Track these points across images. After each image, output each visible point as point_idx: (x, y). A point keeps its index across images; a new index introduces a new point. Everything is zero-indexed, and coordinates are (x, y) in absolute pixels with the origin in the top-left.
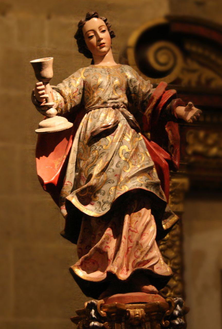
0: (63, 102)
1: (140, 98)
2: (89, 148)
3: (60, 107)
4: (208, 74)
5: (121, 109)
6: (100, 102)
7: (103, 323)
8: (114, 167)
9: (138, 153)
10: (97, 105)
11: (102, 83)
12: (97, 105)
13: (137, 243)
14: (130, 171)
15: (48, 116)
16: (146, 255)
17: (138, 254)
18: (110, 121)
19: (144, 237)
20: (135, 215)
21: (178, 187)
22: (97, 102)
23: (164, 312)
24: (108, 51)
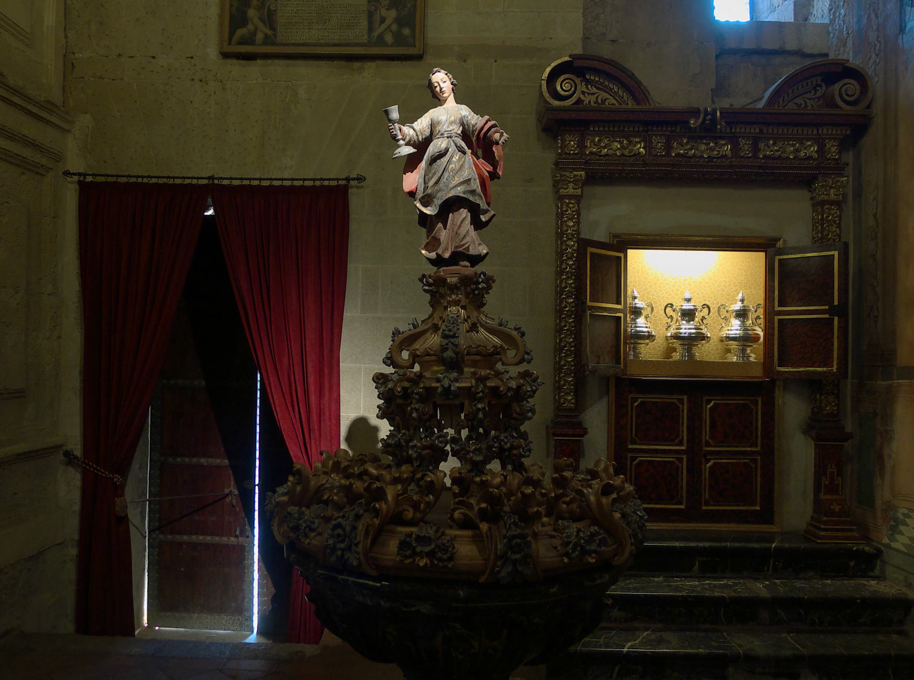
0: (415, 135)
2: (430, 167)
5: (453, 138)
8: (445, 180)
10: (438, 136)
12: (438, 136)
13: (457, 233)
14: (457, 180)
15: (399, 146)
16: (462, 240)
17: (457, 240)
18: (444, 146)
19: (461, 228)
21: (578, 178)
22: (438, 134)
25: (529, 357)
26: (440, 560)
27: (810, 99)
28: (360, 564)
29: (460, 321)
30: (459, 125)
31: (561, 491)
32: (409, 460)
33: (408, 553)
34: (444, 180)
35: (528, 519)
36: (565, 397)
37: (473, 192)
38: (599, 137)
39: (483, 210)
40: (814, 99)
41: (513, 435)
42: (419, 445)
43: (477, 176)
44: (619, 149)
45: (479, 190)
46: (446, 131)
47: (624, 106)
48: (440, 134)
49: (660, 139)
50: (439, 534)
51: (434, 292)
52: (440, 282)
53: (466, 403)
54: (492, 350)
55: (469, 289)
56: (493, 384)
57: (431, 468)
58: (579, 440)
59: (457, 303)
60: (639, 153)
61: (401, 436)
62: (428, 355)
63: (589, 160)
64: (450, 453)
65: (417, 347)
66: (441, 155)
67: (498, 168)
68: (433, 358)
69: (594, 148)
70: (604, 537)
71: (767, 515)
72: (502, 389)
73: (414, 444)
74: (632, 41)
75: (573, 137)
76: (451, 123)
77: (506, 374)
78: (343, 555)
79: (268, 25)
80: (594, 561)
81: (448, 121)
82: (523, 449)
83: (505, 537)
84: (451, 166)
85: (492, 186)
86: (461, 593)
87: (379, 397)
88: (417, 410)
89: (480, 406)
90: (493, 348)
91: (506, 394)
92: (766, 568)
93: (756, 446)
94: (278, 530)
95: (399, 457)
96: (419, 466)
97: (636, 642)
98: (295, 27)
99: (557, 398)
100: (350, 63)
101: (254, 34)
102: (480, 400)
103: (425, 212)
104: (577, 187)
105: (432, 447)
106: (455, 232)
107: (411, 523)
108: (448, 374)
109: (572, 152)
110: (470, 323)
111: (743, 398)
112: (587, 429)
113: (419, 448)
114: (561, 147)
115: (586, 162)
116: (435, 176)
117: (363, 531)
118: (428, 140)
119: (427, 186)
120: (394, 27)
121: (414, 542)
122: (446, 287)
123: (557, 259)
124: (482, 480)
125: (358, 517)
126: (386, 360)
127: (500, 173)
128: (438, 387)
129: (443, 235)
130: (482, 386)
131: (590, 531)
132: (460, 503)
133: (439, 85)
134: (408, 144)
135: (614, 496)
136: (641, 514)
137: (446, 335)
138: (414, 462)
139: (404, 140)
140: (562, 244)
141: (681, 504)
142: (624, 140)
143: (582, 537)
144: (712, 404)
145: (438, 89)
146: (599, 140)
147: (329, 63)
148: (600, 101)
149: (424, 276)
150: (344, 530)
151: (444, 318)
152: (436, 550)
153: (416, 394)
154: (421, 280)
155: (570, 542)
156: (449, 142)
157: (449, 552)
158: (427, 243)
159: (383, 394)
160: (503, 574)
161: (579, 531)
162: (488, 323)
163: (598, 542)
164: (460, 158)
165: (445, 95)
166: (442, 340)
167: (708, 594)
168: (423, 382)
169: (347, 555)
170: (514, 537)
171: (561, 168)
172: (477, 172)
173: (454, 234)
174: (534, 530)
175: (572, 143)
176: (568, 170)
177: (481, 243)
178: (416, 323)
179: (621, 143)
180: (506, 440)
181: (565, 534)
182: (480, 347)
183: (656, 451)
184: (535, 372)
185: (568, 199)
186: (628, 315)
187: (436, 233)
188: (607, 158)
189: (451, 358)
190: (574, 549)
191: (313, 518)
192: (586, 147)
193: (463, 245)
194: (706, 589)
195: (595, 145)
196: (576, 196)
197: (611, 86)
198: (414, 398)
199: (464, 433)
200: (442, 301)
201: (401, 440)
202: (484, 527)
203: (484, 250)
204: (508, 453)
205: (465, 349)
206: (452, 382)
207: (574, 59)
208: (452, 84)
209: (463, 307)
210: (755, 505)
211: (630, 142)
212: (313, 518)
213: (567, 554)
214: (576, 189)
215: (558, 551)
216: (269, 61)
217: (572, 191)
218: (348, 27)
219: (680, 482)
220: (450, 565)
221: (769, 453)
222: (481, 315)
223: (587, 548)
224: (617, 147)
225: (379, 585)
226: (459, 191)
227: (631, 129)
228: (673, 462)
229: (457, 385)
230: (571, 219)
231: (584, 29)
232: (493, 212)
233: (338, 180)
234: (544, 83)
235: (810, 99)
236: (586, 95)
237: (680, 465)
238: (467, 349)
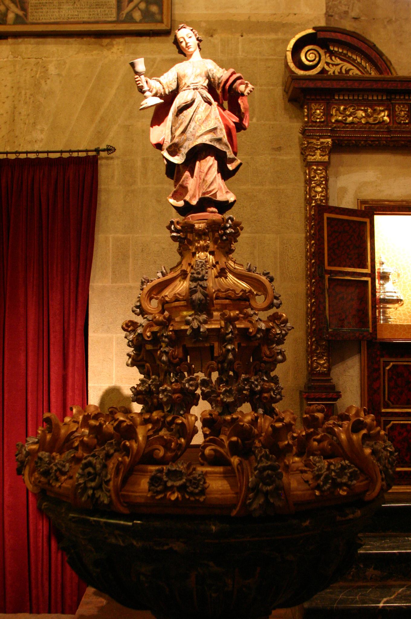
1: (217, 82)
3: (159, 91)
4: (348, 66)
5: (199, 90)
6: (186, 86)
7: (179, 233)
8: (191, 130)
9: (210, 119)
10: (184, 88)
11: (179, 74)
12: (184, 88)
13: (204, 180)
14: (203, 129)
15: (146, 97)
16: (209, 187)
17: (204, 187)
20: (203, 162)
21: (325, 145)
22: (184, 86)
23: (220, 225)
24: (195, 51)
25: (278, 302)
26: (192, 494)
28: (111, 502)
29: (208, 266)
30: (205, 78)
31: (312, 430)
32: (159, 406)
33: (160, 488)
34: (190, 129)
36: (318, 361)
37: (219, 140)
38: (344, 105)
39: (230, 158)
41: (263, 379)
42: (169, 388)
43: (223, 126)
44: (364, 117)
45: (225, 139)
46: (192, 83)
47: (367, 75)
48: (186, 86)
49: (403, 107)
50: (191, 470)
51: (182, 238)
52: (188, 228)
53: (216, 345)
54: (241, 294)
55: (217, 235)
56: (242, 326)
57: (182, 412)
58: (333, 404)
59: (204, 249)
60: (384, 121)
61: (152, 382)
62: (177, 300)
63: (335, 127)
64: (201, 397)
65: (167, 294)
66: (187, 106)
67: (244, 119)
68: (182, 303)
69: (339, 117)
70: (354, 470)
72: (251, 330)
73: (164, 388)
74: (374, 19)
75: (318, 106)
76: (197, 76)
77: (254, 315)
78: (93, 494)
79: (19, 7)
80: (345, 493)
81: (194, 74)
82: (274, 392)
83: (256, 469)
84: (197, 116)
85: (240, 137)
86: (214, 528)
87: (129, 346)
88: (166, 353)
89: (229, 347)
90: (242, 292)
91: (255, 335)
94: (30, 480)
95: (150, 404)
96: (169, 411)
97: (392, 597)
98: (46, 7)
99: (309, 362)
100: (99, 40)
102: (230, 341)
104: (324, 154)
105: (183, 391)
106: (202, 180)
107: (162, 461)
108: (197, 316)
109: (318, 120)
110: (218, 268)
112: (340, 392)
113: (169, 391)
114: (307, 116)
115: (332, 131)
116: (182, 125)
117: (114, 469)
118: (174, 93)
119: (174, 135)
120: (143, 6)
121: (165, 477)
122: (194, 234)
123: (307, 225)
124: (232, 419)
125: (108, 456)
126: (135, 309)
127: (246, 124)
128: (187, 330)
129: (191, 183)
130: (231, 327)
131: (341, 464)
132: (211, 441)
133: (185, 40)
134: (155, 95)
135: (364, 431)
136: (391, 450)
137: (194, 277)
138: (165, 407)
139: (151, 92)
142: (369, 108)
143: (333, 470)
145: (183, 44)
146: (344, 109)
147: (79, 40)
148: (344, 71)
149: (172, 223)
150: (94, 468)
151: (192, 265)
152: (188, 484)
153: (166, 337)
155: (322, 475)
156: (195, 93)
157: (201, 486)
158: (175, 192)
159: (132, 341)
160: (255, 506)
161: (330, 464)
162: (237, 269)
163: (348, 475)
164: (206, 109)
165: (190, 50)
166: (191, 283)
168: (172, 325)
169: (98, 494)
170: (265, 469)
171: (308, 136)
172: (223, 122)
173: (201, 181)
174: (285, 463)
175: (318, 111)
176: (314, 137)
177: (229, 191)
178: (164, 271)
179: (365, 111)
180: (256, 383)
181: (316, 468)
182: (228, 291)
184: (284, 315)
185: (315, 165)
186: (377, 281)
187: (183, 181)
188: (353, 125)
189: (199, 300)
190: (325, 483)
191: (64, 462)
192: (332, 115)
193: (211, 192)
195: (341, 113)
197: (354, 57)
198: (164, 342)
199: (215, 376)
200: (190, 247)
201: (151, 386)
202: (235, 460)
203: (231, 198)
204: (258, 396)
205: (214, 292)
206: (201, 323)
208: (198, 39)
209: (212, 253)
211: (375, 110)
212: (64, 462)
213: (318, 487)
214: (323, 156)
215: (309, 485)
216: (20, 40)
217: (320, 157)
218: (98, 7)
222: (230, 262)
223: (339, 480)
224: (362, 115)
225: (130, 524)
226: (206, 139)
229: (207, 326)
230: (319, 185)
231: (327, 7)
232: (239, 161)
233: (87, 151)
234: (289, 55)
236: (331, 66)
238: (216, 293)
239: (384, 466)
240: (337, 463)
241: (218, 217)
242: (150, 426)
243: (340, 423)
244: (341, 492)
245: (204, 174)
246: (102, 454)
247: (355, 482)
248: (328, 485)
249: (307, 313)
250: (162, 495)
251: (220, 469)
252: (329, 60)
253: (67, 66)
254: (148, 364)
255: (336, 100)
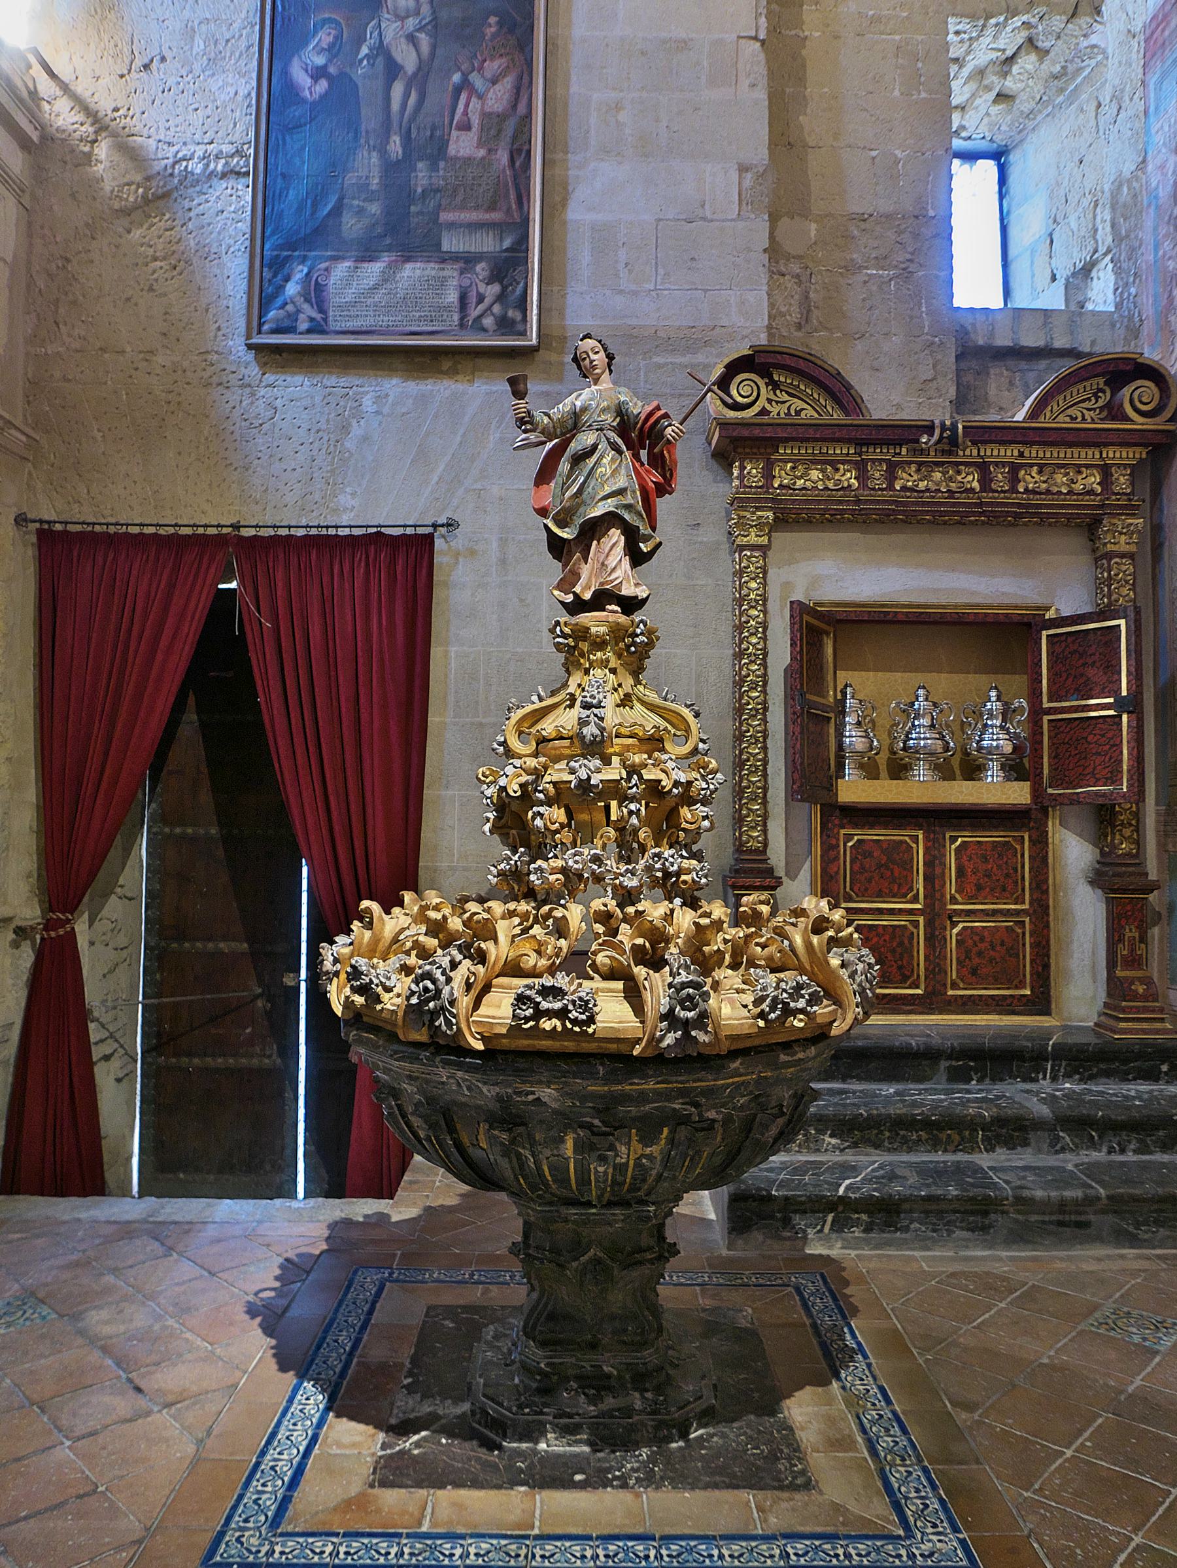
13: (603, 564)
16: (610, 574)
26: (575, 1022)
27: (1089, 410)
29: (606, 689)
31: (753, 929)
35: (705, 964)
39: (644, 535)
40: (1094, 409)
45: (640, 507)
52: (582, 633)
56: (652, 777)
59: (604, 664)
63: (779, 495)
71: (1041, 1003)
72: (663, 783)
76: (604, 410)
80: (802, 1024)
92: (1041, 1076)
93: (1023, 903)
101: (294, 317)
103: (560, 534)
107: (534, 974)
111: (1002, 834)
124: (636, 911)
125: (454, 965)
135: (831, 933)
140: (741, 615)
141: (918, 987)
144: (958, 843)
149: (558, 623)
152: (570, 1007)
154: (552, 631)
160: (664, 1044)
161: (780, 980)
164: (613, 460)
167: (958, 1109)
170: (684, 985)
179: (823, 471)
183: (880, 911)
190: (773, 1008)
193: (612, 581)
194: (955, 1104)
196: (762, 546)
203: (642, 592)
207: (756, 352)
209: (613, 671)
210: (1024, 987)
213: (762, 1015)
219: (915, 954)
220: (590, 1030)
221: (1041, 911)
223: (792, 1005)
227: (838, 452)
228: (905, 926)
235: (1089, 410)
237: (915, 931)
239: (860, 985)
240: (790, 978)
241: (622, 619)
242: (516, 920)
243: (793, 920)
244: (796, 1023)
245: (603, 556)
246: (446, 962)
247: (815, 1008)
248: (778, 1012)
249: (734, 763)
250: (532, 1023)
251: (620, 985)
252: (772, 397)
253: (390, 399)
254: (514, 832)
255: (781, 455)
